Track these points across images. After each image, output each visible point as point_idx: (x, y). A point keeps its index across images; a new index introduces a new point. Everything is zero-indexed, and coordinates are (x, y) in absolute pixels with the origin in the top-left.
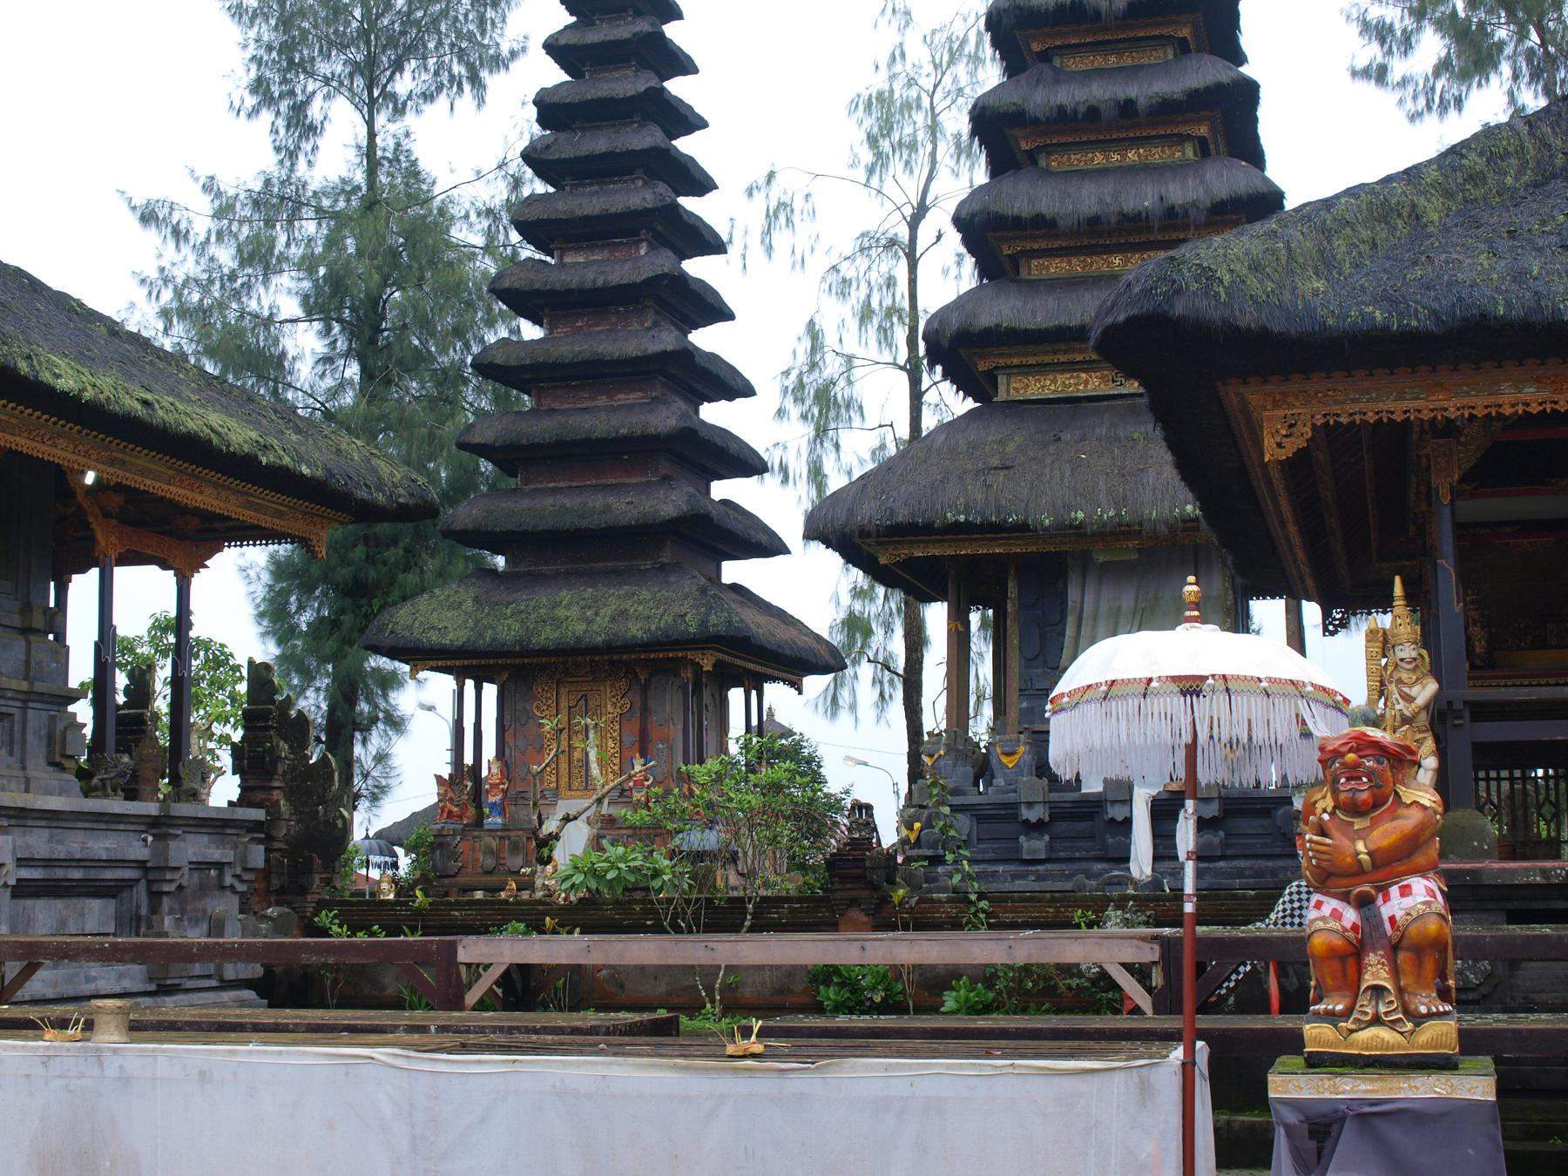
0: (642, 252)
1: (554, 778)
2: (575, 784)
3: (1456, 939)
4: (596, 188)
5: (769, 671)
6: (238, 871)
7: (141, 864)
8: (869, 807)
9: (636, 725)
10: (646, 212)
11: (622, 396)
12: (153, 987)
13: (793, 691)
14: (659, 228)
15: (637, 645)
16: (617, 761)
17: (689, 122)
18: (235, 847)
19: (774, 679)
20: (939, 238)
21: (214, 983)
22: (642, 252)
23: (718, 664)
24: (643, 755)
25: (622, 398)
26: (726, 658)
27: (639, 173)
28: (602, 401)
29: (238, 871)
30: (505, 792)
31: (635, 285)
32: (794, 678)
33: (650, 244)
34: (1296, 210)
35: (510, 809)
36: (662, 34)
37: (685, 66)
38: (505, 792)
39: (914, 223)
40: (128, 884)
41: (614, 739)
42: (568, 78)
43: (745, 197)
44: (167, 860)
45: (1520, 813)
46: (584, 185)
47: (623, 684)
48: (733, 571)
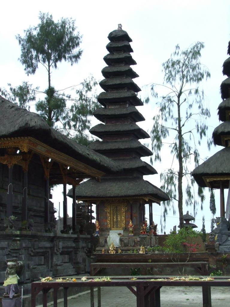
0: (127, 106)
1: (110, 225)
4: (116, 91)
5: (153, 200)
6: (87, 248)
7: (74, 248)
10: (129, 97)
11: (123, 139)
12: (76, 273)
14: (131, 101)
17: (135, 75)
20: (185, 100)
21: (84, 272)
22: (127, 106)
24: (132, 220)
25: (123, 139)
27: (126, 88)
28: (119, 140)
30: (99, 228)
31: (127, 114)
32: (158, 202)
33: (129, 105)
34: (132, 80)
36: (109, 52)
37: (134, 63)
39: (179, 97)
40: (71, 251)
41: (124, 216)
42: (108, 66)
43: (9, 83)
46: (113, 91)
48: (146, 178)
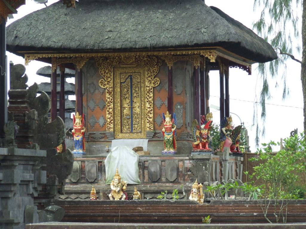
1: (112, 126)
2: (125, 129)
3: (120, 215)
8: (291, 133)
9: (165, 94)
13: (245, 73)
15: (172, 47)
16: (151, 116)
18: (34, 171)
19: (234, 65)
23: (218, 58)
26: (221, 55)
29: (36, 185)
30: (83, 134)
35: (86, 144)
38: (83, 134)
41: (150, 102)
44: (13, 180)
45: (183, 139)
47: (156, 68)
